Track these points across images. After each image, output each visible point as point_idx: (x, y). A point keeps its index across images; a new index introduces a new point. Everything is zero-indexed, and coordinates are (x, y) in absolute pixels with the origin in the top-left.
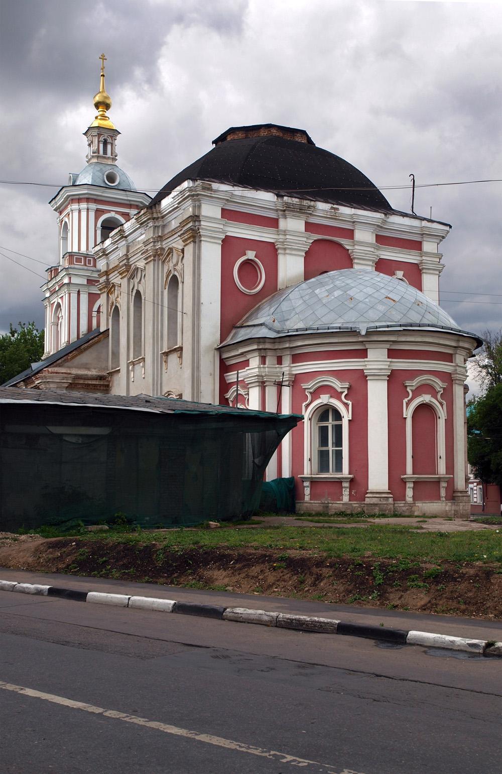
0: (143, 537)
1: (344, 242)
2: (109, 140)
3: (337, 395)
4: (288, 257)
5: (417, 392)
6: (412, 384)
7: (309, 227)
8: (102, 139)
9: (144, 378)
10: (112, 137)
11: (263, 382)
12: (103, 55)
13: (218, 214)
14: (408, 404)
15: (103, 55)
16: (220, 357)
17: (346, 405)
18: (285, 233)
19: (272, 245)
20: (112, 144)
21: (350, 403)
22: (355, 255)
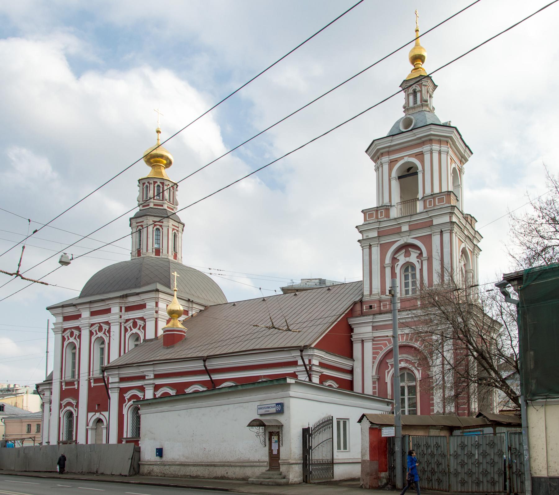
17: (75, 410)
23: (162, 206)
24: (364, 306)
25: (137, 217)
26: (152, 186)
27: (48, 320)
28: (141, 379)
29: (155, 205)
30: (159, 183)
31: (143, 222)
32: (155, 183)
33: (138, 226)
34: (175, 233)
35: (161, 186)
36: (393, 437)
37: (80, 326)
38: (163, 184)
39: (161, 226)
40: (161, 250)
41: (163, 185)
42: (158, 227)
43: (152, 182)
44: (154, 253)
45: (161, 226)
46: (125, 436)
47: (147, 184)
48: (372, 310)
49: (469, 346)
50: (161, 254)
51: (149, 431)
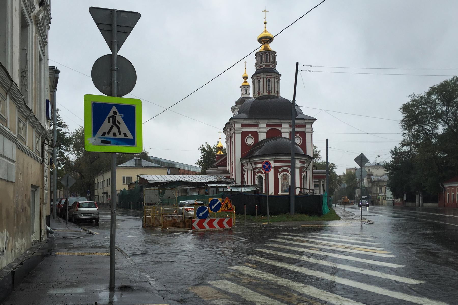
0: (299, 235)
1: (280, 129)
2: (247, 89)
3: (262, 173)
4: (261, 135)
5: (282, 172)
6: (281, 170)
7: (267, 126)
8: (245, 89)
9: (379, 156)
10: (248, 88)
11: (247, 170)
12: (245, 62)
13: (240, 126)
14: (279, 175)
15: (245, 62)
16: (241, 163)
17: (264, 175)
18: (260, 128)
19: (257, 132)
20: (248, 90)
21: (265, 175)
22: (282, 132)
23: (270, 66)
24: (449, 189)
25: (256, 73)
26: (264, 56)
27: (327, 140)
28: (41, 75)
29: (266, 66)
30: (267, 53)
31: (261, 76)
32: (265, 53)
33: (258, 79)
34: (277, 81)
35: (269, 54)
36: (141, 164)
37: (258, 132)
38: (269, 53)
39: (270, 78)
40: (271, 92)
41: (269, 54)
42: (269, 78)
43: (264, 53)
44: (267, 93)
45: (270, 78)
46: (241, 185)
47: (261, 54)
48: (291, 153)
49: (265, 244)
50: (271, 93)
51: (370, 266)
